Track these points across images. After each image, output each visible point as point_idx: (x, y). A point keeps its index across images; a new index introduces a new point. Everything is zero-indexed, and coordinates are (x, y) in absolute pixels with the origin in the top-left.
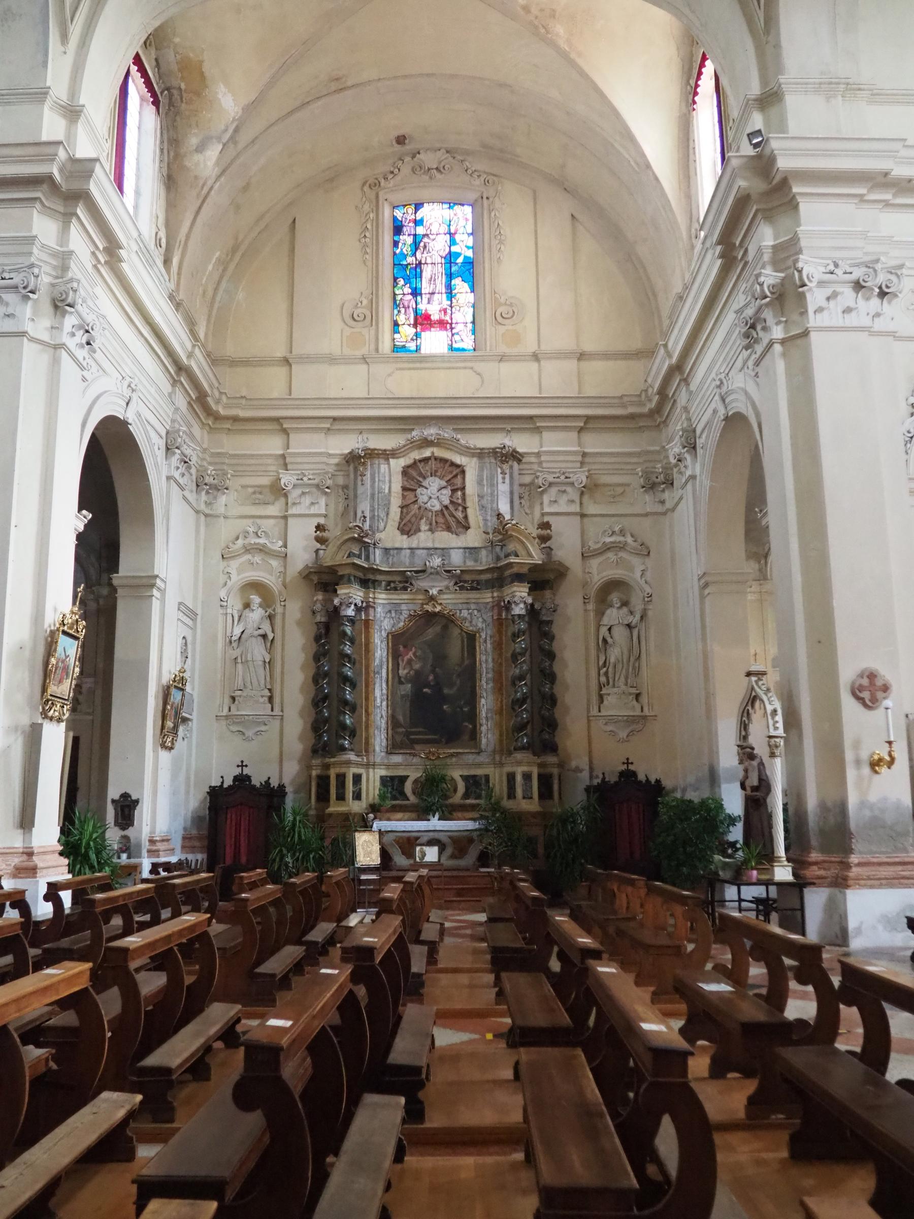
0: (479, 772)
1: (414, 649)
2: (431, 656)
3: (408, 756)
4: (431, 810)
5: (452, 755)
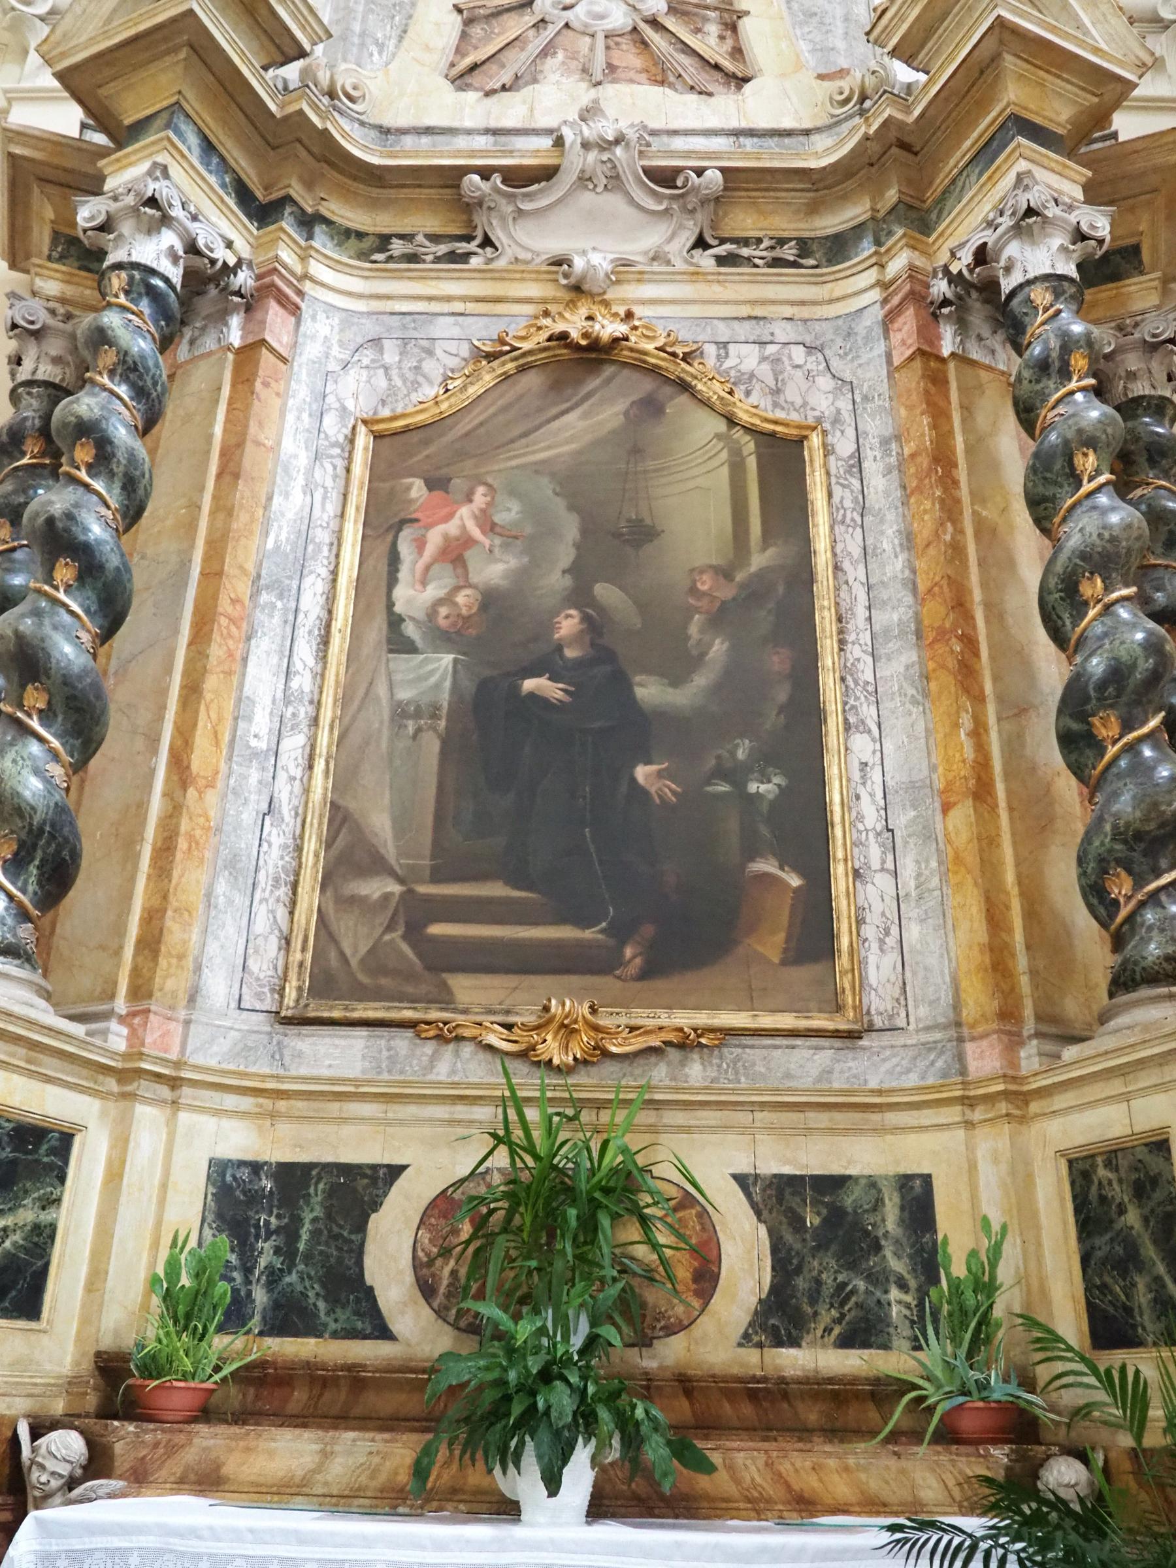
0: (863, 1156)
1: (480, 497)
2: (571, 528)
3: (402, 1041)
4: (531, 1420)
5: (686, 1043)
